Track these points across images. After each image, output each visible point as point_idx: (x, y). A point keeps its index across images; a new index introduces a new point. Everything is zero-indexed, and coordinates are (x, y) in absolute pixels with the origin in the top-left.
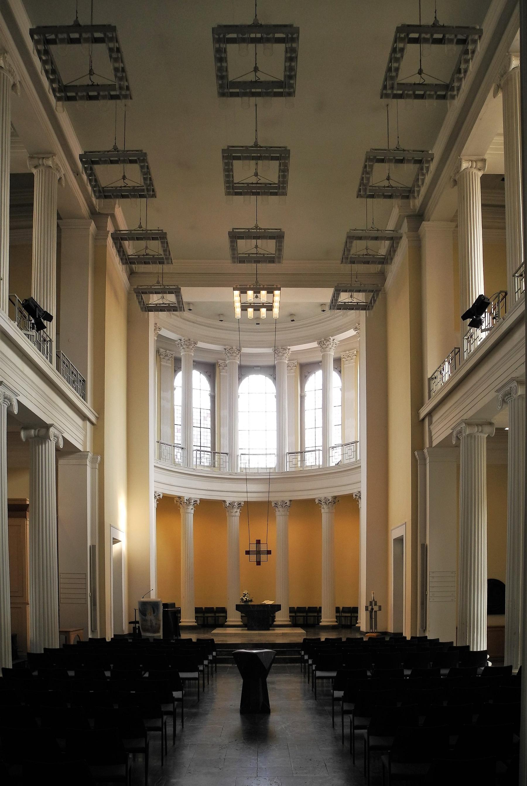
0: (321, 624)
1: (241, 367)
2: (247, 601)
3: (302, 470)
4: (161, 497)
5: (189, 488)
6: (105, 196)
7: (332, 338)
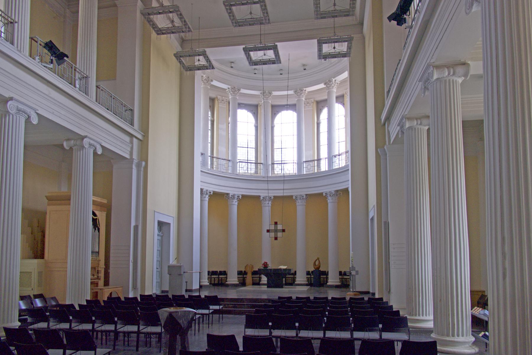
0: (328, 284)
1: (273, 106)
3: (314, 173)
4: (212, 193)
6: (239, 25)
7: (334, 80)
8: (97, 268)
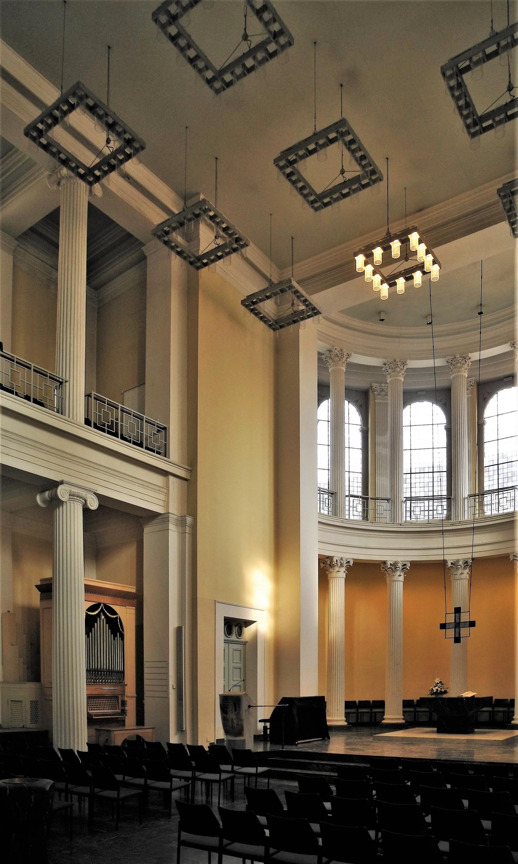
2: (436, 693)
5: (386, 549)
8: (120, 697)
